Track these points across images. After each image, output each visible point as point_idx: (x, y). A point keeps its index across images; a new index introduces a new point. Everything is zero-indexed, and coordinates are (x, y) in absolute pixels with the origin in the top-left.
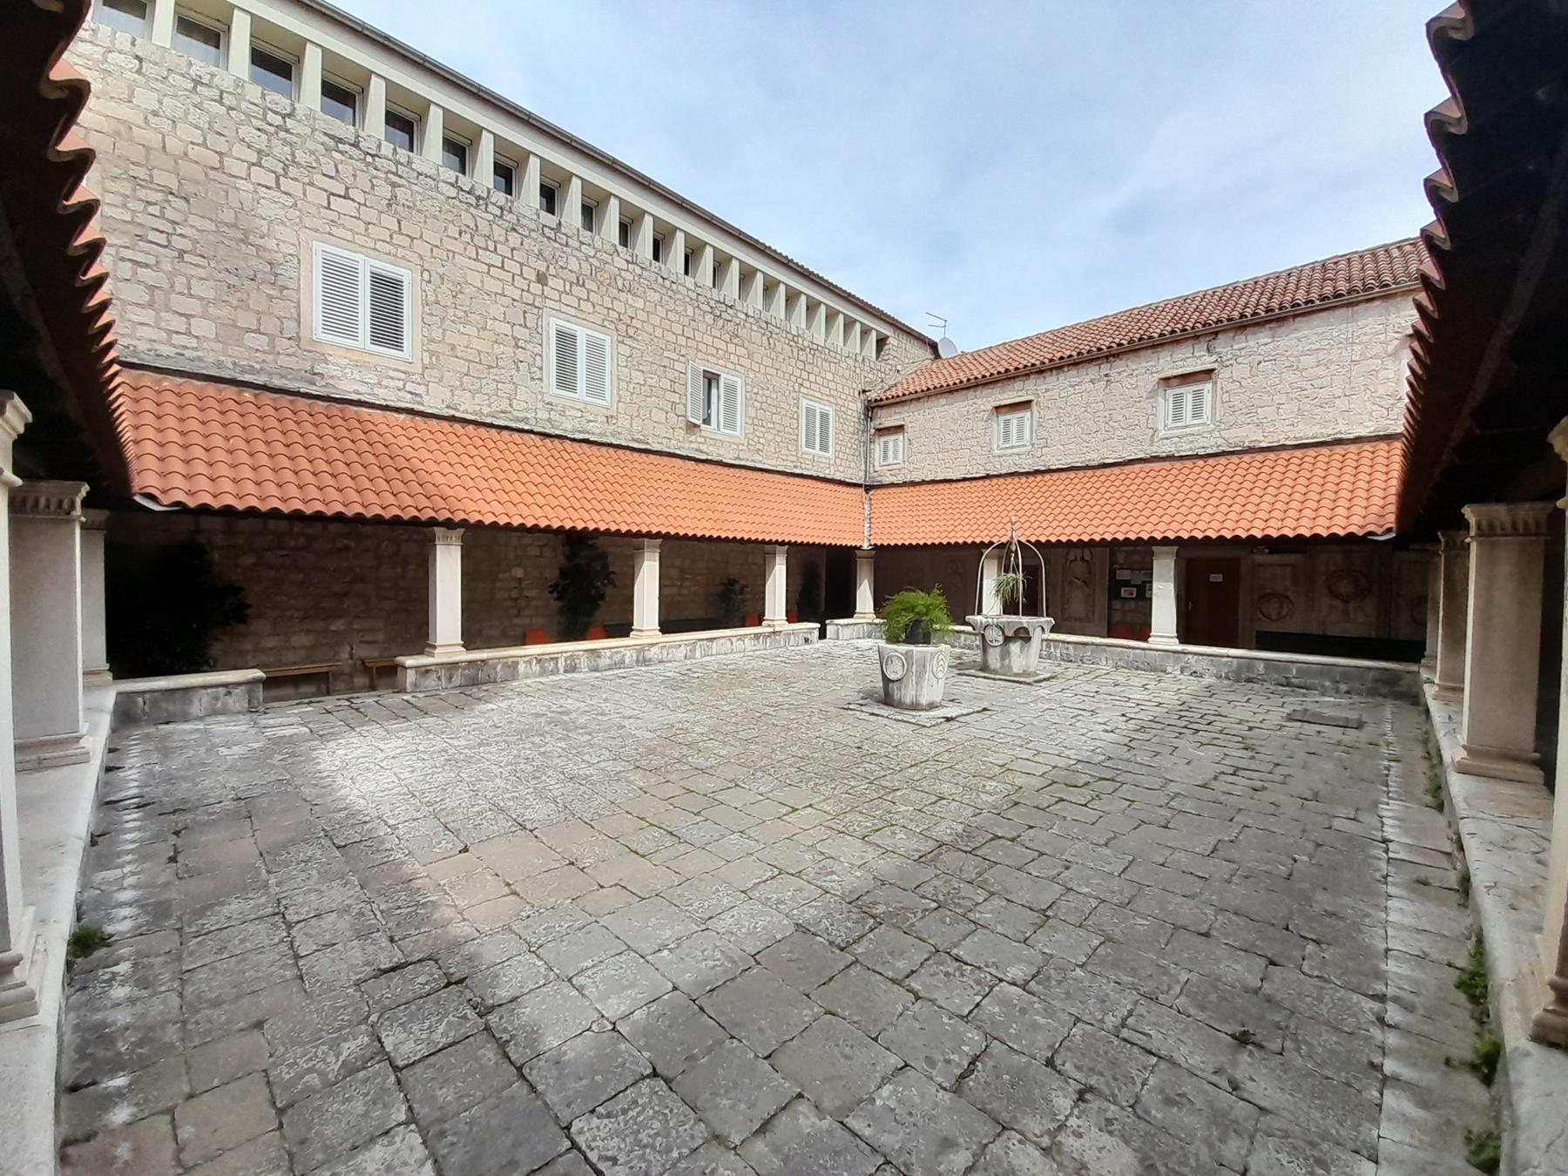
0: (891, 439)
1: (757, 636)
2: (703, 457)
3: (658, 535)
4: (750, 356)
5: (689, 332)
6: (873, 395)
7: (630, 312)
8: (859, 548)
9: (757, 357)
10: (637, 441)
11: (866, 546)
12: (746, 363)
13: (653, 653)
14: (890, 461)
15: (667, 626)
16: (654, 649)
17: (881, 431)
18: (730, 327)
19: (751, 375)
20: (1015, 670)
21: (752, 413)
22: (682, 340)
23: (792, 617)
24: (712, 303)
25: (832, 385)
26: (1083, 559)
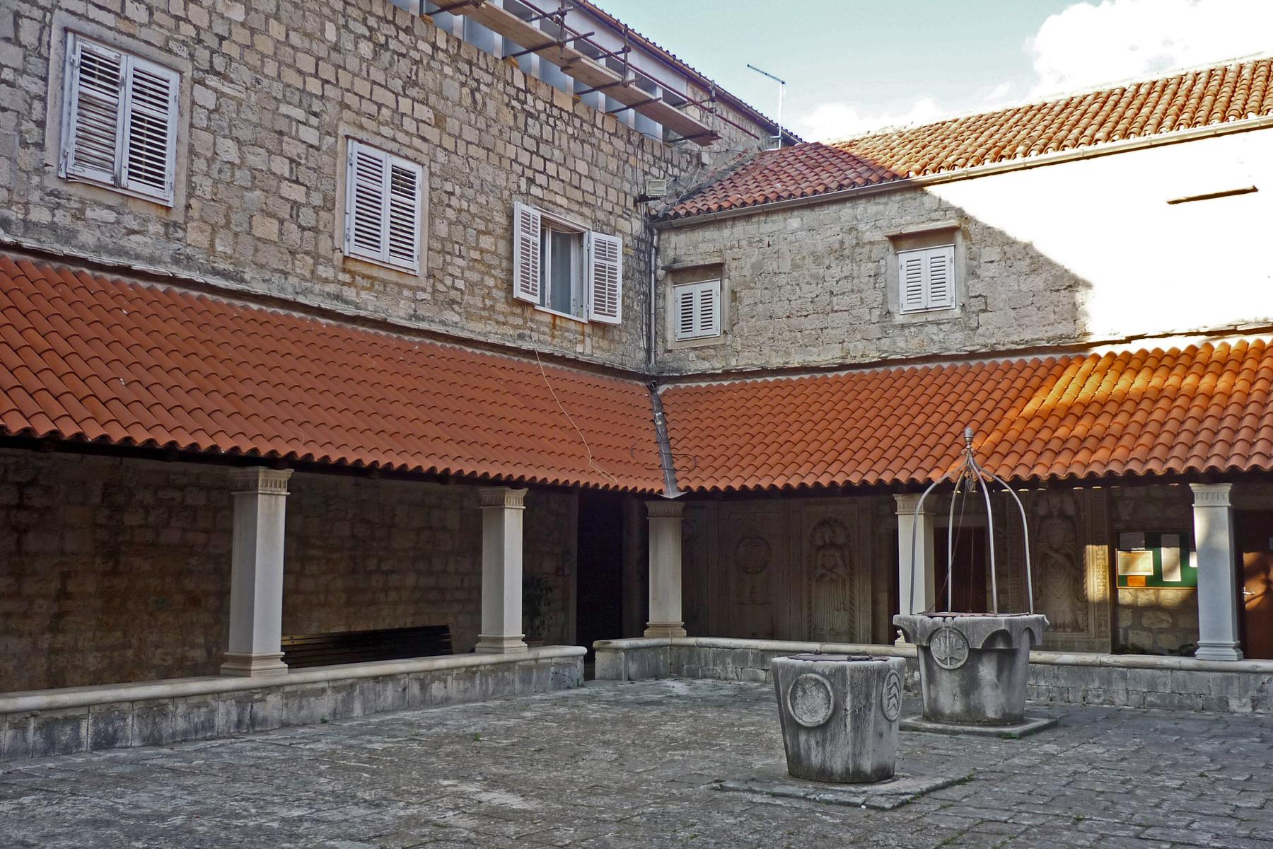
0: (697, 289)
1: (470, 672)
2: (350, 311)
3: (290, 461)
4: (440, 121)
5: (327, 72)
6: (658, 207)
7: (220, 28)
8: (657, 497)
9: (452, 125)
10: (224, 274)
11: (671, 494)
12: (432, 133)
13: (272, 707)
14: (697, 330)
15: (295, 657)
16: (273, 699)
17: (680, 273)
18: (404, 66)
19: (441, 156)
20: (991, 714)
21: (442, 229)
22: (314, 86)
23: (533, 635)
24: (372, 22)
25: (587, 185)
26: (1063, 515)
